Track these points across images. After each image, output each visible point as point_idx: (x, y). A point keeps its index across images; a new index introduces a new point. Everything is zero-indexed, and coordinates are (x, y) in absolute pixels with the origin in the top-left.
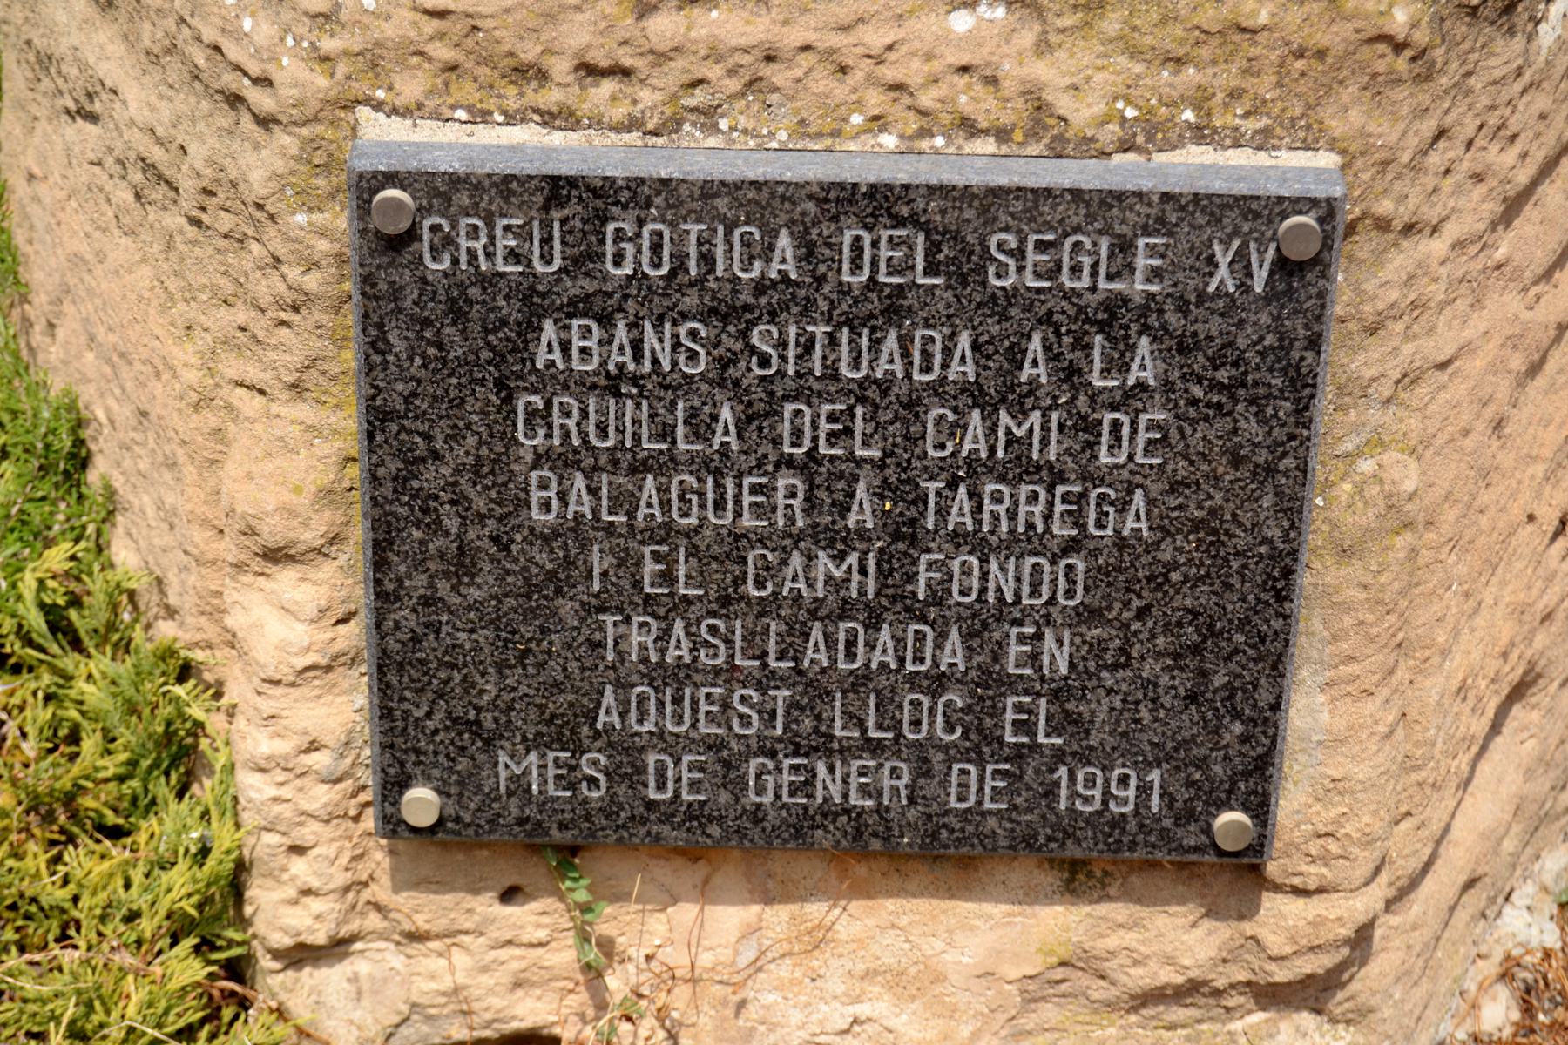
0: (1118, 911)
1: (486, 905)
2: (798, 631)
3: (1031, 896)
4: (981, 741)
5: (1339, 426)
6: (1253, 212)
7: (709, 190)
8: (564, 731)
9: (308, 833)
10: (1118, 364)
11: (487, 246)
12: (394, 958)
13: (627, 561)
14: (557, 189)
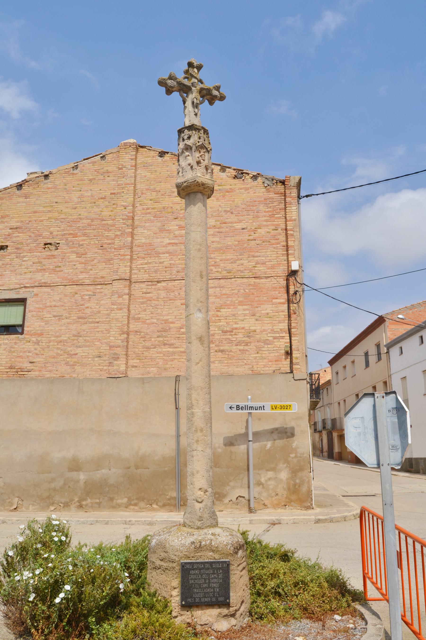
0: (222, 609)
1: (186, 612)
2: (204, 589)
3: (217, 609)
4: (214, 596)
5: (231, 576)
6: (226, 562)
7: (199, 562)
8: (191, 597)
9: (176, 607)
10: (220, 571)
11: (188, 566)
12: (180, 617)
13: (195, 585)
14: (191, 563)
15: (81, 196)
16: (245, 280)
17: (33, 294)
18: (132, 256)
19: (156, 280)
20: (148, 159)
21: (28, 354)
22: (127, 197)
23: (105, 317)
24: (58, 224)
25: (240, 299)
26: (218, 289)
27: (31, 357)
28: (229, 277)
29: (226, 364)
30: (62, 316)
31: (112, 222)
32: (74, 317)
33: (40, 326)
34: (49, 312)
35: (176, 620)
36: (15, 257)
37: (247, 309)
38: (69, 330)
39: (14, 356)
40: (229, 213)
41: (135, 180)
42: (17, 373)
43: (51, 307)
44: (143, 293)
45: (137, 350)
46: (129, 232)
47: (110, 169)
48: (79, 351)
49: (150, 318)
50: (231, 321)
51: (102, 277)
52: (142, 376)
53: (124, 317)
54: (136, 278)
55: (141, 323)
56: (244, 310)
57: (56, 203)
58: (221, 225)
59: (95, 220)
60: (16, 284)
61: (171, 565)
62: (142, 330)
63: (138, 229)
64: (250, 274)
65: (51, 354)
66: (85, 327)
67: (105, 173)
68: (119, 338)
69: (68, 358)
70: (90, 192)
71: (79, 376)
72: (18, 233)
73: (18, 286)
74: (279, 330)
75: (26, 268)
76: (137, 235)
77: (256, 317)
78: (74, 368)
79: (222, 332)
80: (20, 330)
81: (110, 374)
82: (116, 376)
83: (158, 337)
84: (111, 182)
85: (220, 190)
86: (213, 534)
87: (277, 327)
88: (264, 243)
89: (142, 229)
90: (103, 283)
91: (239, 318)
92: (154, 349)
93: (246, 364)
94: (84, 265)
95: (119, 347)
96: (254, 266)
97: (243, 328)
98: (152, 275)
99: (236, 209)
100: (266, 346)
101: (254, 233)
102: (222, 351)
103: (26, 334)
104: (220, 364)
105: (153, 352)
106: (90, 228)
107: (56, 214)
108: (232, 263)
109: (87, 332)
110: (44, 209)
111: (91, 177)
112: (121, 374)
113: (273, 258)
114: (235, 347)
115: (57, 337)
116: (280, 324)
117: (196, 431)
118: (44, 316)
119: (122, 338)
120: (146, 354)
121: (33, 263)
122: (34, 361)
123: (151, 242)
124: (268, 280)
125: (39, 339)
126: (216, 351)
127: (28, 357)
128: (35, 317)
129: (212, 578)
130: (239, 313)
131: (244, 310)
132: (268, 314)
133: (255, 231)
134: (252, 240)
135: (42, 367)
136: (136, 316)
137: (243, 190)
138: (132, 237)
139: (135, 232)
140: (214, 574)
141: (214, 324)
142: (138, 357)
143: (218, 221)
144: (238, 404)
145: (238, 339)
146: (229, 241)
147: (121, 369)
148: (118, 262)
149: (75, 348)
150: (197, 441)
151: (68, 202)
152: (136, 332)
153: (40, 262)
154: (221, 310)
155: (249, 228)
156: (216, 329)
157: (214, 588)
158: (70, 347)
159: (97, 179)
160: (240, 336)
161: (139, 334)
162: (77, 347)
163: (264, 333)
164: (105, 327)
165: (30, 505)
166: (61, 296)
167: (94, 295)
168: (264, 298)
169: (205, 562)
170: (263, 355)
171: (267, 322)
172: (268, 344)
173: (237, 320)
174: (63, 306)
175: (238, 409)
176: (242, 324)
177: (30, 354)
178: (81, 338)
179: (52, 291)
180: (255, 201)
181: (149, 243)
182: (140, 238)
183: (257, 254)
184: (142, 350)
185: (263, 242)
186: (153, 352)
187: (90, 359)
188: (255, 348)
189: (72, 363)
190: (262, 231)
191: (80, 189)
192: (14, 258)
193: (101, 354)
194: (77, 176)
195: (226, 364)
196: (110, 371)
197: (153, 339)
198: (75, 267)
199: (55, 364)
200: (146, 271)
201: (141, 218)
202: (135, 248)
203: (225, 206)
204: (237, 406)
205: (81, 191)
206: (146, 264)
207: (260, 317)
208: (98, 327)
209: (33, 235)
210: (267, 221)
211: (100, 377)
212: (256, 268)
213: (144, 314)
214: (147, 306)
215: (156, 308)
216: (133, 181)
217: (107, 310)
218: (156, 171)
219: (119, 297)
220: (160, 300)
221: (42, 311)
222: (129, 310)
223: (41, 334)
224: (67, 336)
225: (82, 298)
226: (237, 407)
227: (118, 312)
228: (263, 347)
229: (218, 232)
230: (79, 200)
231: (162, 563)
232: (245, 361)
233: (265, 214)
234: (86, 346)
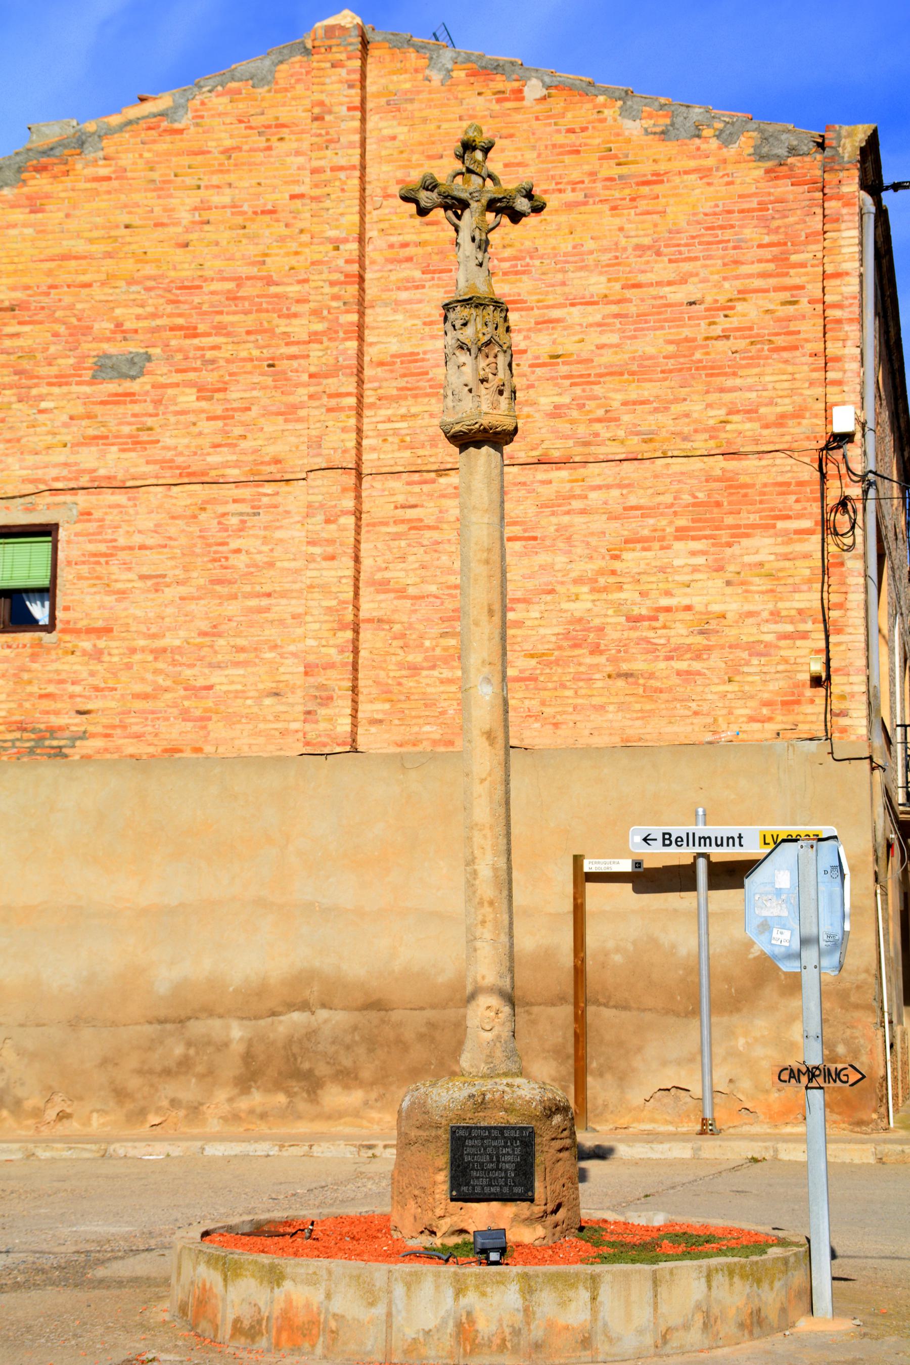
4: (506, 1185)
8: (467, 1184)
11: (461, 1133)
15: (203, 206)
16: (696, 464)
17: (75, 512)
18: (360, 397)
19: (435, 467)
20: (402, 77)
21: (71, 689)
22: (340, 211)
23: (290, 579)
24: (139, 297)
25: (682, 522)
26: (615, 493)
27: (80, 696)
28: (646, 455)
29: (640, 715)
30: (164, 576)
31: (297, 288)
32: (199, 578)
33: (102, 607)
34: (127, 567)
35: (442, 1222)
36: (14, 399)
37: (703, 553)
38: (188, 618)
39: (31, 694)
40: (649, 253)
41: (363, 156)
42: (43, 745)
43: (131, 548)
44: (396, 508)
45: (382, 674)
46: (351, 323)
47: (284, 114)
48: (216, 678)
49: (418, 580)
50: (654, 586)
51: (277, 461)
52: (399, 750)
53: (344, 581)
54: (376, 463)
55: (392, 595)
56: (693, 553)
57: (127, 227)
58: (625, 291)
59: (249, 283)
60: (24, 481)
61: (433, 1133)
62: (396, 617)
63: (378, 310)
64: (712, 443)
65: (138, 688)
66: (232, 608)
67: (269, 127)
68: (331, 642)
69: (187, 698)
70: (227, 191)
71: (221, 750)
72: (20, 323)
73: (30, 488)
74: (793, 613)
75: (49, 433)
76: (374, 328)
77: (729, 576)
78: (205, 727)
79: (628, 619)
80: (39, 611)
81: (307, 744)
82: (326, 750)
83: (444, 635)
84: (289, 160)
85: (621, 177)
86: (508, 1085)
87: (788, 605)
88: (754, 349)
89: (388, 310)
90: (278, 477)
91: (677, 578)
92: (431, 672)
93: (696, 713)
94: (220, 423)
95: (332, 666)
96: (722, 418)
97: (688, 608)
98: (421, 452)
99: (671, 239)
100: (755, 661)
101: (726, 316)
102: (627, 675)
103: (63, 631)
104: (620, 714)
105: (428, 681)
106: (234, 308)
107: (129, 265)
108: (656, 410)
109: (240, 623)
110: (94, 248)
111: (228, 143)
112: (339, 745)
113: (781, 393)
114: (662, 665)
115: (154, 636)
116: (797, 596)
117: (481, 903)
118: (113, 577)
119: (339, 641)
120: (410, 683)
121: (72, 418)
122: (89, 707)
123: (416, 351)
124: (764, 463)
125: (101, 644)
126: (609, 676)
127: (72, 696)
128: (87, 578)
129: (504, 1155)
130: (677, 562)
131: (693, 553)
132: (761, 564)
133: (727, 308)
134: (718, 338)
135: (114, 727)
136: (378, 576)
137: (693, 177)
138: (361, 338)
139: (368, 319)
140: (505, 1146)
141: (604, 596)
142: (386, 693)
143: (616, 280)
144: (667, 829)
145: (672, 640)
146: (653, 343)
147: (339, 729)
148: (323, 418)
149: (207, 671)
150: (483, 922)
151: (162, 225)
152: (380, 621)
153: (89, 416)
154: (626, 555)
155: (709, 299)
156: (610, 612)
157: (506, 1171)
158: (191, 666)
159: (246, 147)
160: (680, 632)
161: (387, 627)
162: (210, 665)
163: (750, 621)
164: (290, 609)
165: (92, 1112)
166: (160, 516)
167: (255, 514)
168: (752, 516)
169: (492, 1128)
170: (747, 688)
171: (759, 588)
172: (760, 654)
173: (670, 586)
174: (165, 546)
175: (667, 842)
176: (686, 594)
177: (77, 689)
178: (221, 642)
179: (131, 503)
180: (730, 212)
181: (412, 354)
182: (384, 339)
183: (730, 382)
184: (398, 674)
185: (752, 343)
186: (428, 681)
187: (249, 702)
188: (723, 665)
189: (198, 713)
190: (749, 311)
191: (195, 182)
192: (10, 403)
193: (281, 685)
194: (185, 136)
195: (640, 715)
196: (309, 737)
197: (427, 643)
198: (195, 430)
199: (150, 716)
200: (403, 441)
201: (386, 274)
202: (368, 372)
203: (637, 229)
204: (664, 834)
205: (199, 187)
206: (403, 418)
207: (739, 573)
208: (268, 610)
209: (62, 329)
210: (764, 275)
211: (282, 753)
212: (729, 427)
213: (402, 570)
214: (409, 545)
215: (436, 551)
216: (356, 160)
217: (294, 560)
218: (425, 120)
219: (328, 521)
220: (445, 526)
221: (107, 563)
222: (357, 559)
223: (107, 630)
224: (182, 633)
225: (219, 523)
226: (664, 839)
227: (325, 564)
228: (748, 663)
229: (616, 316)
230: (197, 218)
231: (421, 1133)
232: (694, 706)
233: (761, 251)
234: (237, 664)
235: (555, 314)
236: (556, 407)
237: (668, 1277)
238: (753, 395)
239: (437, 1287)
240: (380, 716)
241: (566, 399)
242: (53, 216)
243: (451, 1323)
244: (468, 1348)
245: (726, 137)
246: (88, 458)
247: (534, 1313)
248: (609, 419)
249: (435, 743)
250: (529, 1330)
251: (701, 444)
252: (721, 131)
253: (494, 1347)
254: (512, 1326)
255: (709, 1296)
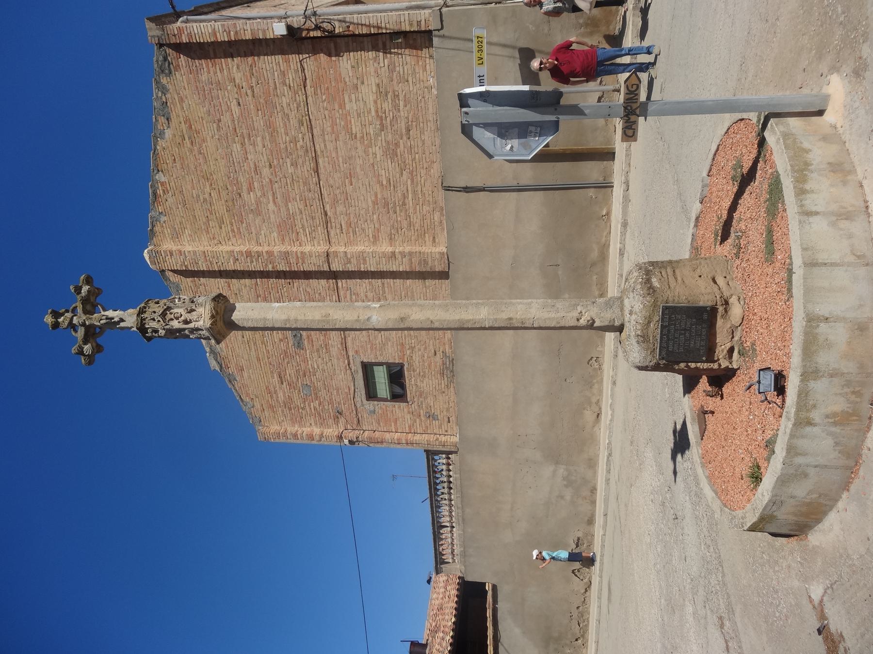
8: (699, 350)
16: (310, 99)
25: (337, 107)
37: (349, 96)
45: (413, 238)
56: (351, 101)
64: (300, 93)
82: (447, 262)
97: (375, 102)
100: (397, 69)
108: (288, 119)
120: (417, 226)
125: (407, 347)
132: (353, 67)
140: (675, 325)
153: (318, 351)
155: (236, 96)
157: (692, 325)
177: (426, 355)
206: (304, 230)
232: (420, 98)
235: (252, 166)
236: (292, 165)
237: (810, 253)
238: (276, 73)
239: (803, 437)
240: (431, 238)
241: (288, 160)
242: (243, 362)
243: (833, 429)
244: (855, 418)
245: (164, 90)
246: (334, 351)
247: (834, 369)
248: (295, 141)
249: (442, 215)
250: (848, 373)
251: (301, 98)
252: (162, 92)
253: (858, 400)
254: (843, 386)
255: (825, 214)
